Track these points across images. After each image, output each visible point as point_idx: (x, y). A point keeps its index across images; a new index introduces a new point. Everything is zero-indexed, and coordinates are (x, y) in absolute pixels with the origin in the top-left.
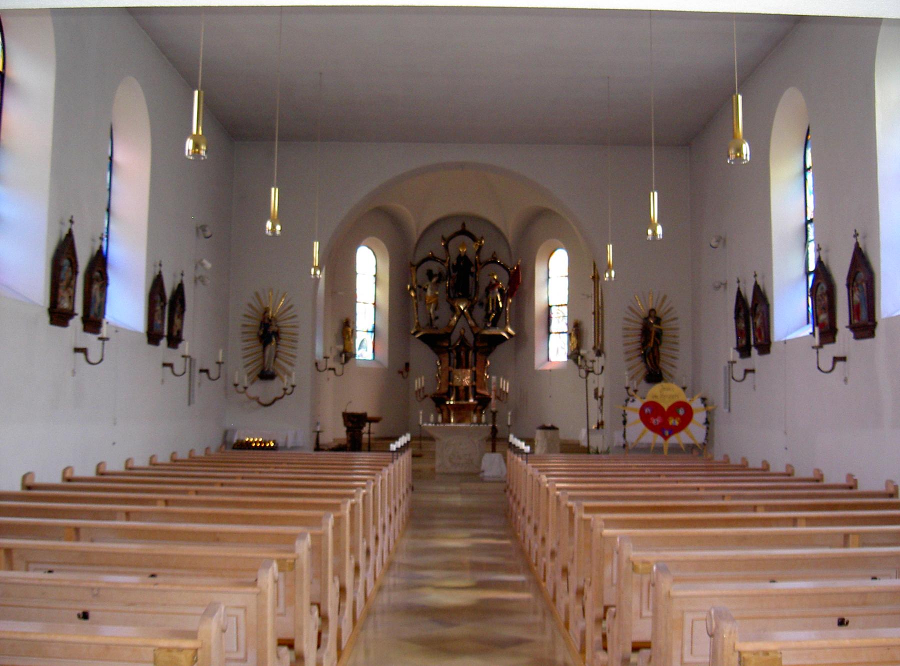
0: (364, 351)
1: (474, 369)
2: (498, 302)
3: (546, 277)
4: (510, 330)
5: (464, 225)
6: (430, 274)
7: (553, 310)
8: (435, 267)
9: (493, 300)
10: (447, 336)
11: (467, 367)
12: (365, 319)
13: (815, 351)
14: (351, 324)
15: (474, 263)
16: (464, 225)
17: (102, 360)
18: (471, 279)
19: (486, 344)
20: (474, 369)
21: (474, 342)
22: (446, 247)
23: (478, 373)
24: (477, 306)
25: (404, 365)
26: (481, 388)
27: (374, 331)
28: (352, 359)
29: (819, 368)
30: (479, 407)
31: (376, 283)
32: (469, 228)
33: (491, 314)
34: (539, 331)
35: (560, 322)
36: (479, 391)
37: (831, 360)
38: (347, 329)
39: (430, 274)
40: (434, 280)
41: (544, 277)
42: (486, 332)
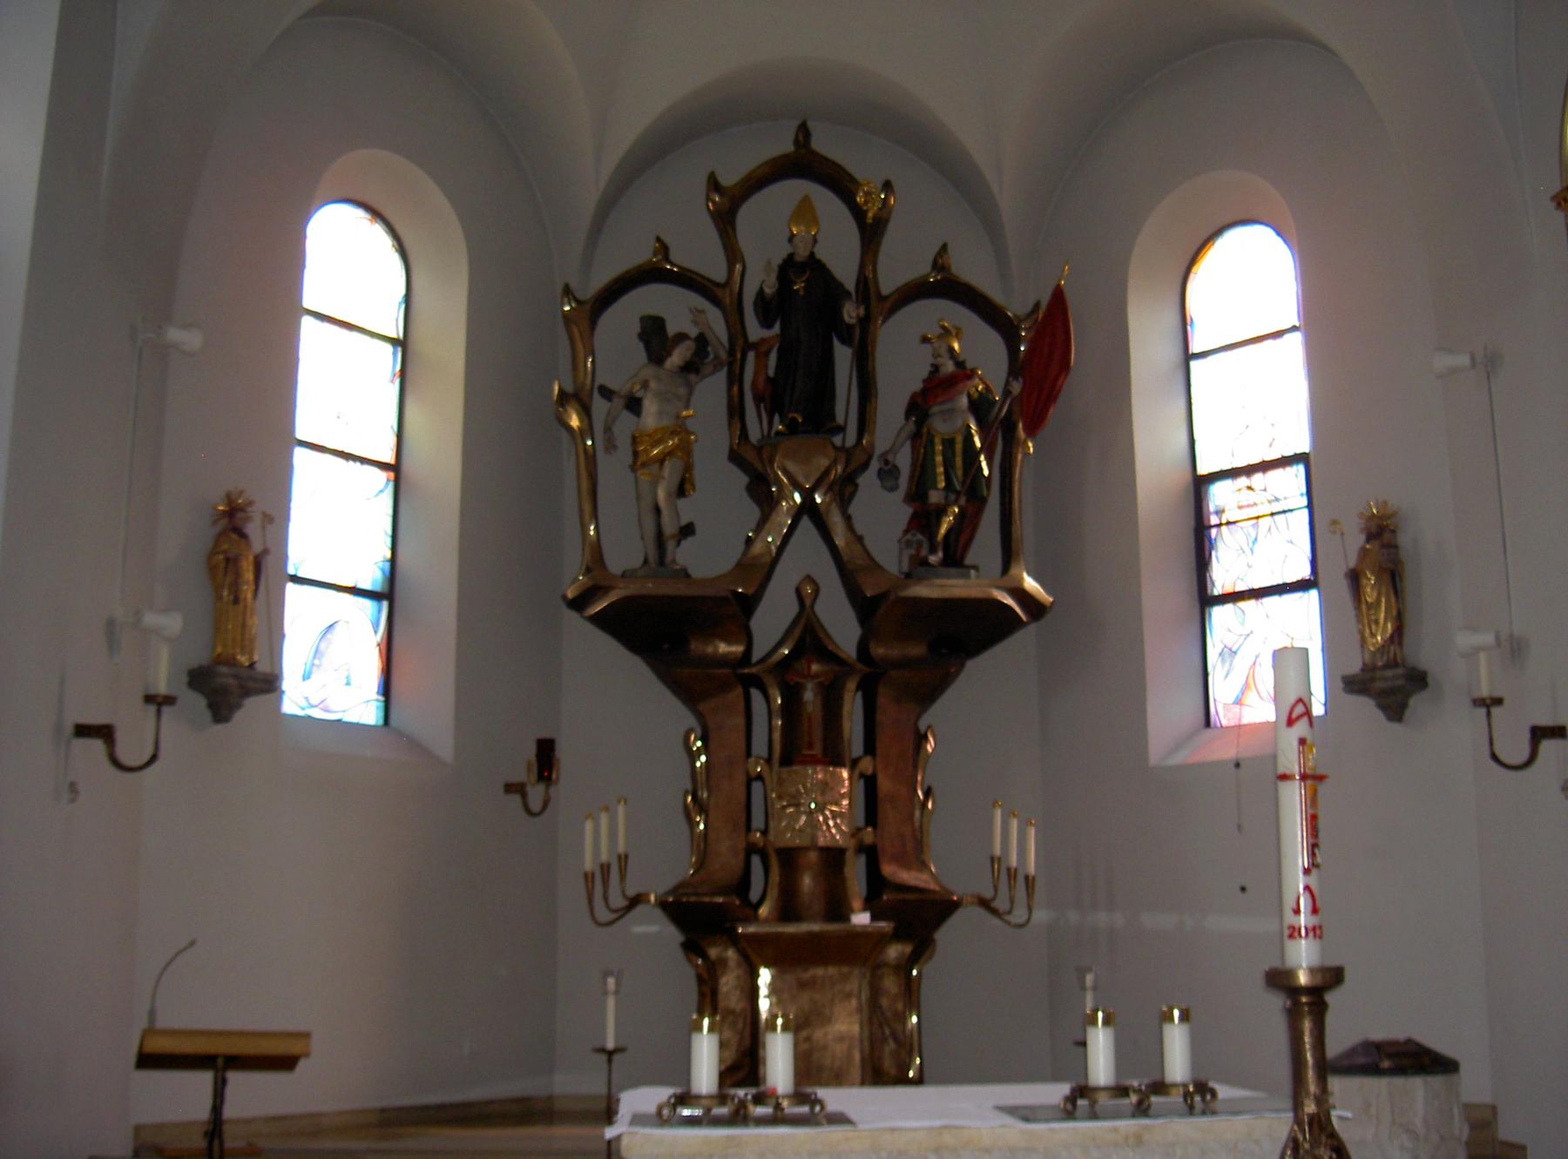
0: (329, 664)
1: (867, 765)
2: (971, 455)
3: (1173, 353)
4: (1030, 583)
5: (804, 132)
6: (654, 336)
7: (1220, 495)
8: (678, 309)
9: (949, 444)
10: (734, 609)
11: (834, 756)
12: (336, 525)
13: (1483, 711)
14: (253, 529)
15: (850, 285)
16: (804, 132)
17: (154, 758)
18: (843, 356)
19: (917, 650)
20: (867, 765)
21: (863, 647)
22: (725, 220)
23: (884, 784)
24: (868, 481)
25: (531, 752)
26: (903, 861)
27: (387, 594)
28: (252, 704)
29: (1494, 757)
30: (894, 952)
31: (403, 374)
32: (825, 144)
33: (941, 511)
34: (1160, 592)
35: (1263, 538)
36: (889, 870)
37: (1527, 736)
38: (238, 556)
39: (654, 336)
40: (677, 358)
41: (1168, 353)
42: (921, 591)
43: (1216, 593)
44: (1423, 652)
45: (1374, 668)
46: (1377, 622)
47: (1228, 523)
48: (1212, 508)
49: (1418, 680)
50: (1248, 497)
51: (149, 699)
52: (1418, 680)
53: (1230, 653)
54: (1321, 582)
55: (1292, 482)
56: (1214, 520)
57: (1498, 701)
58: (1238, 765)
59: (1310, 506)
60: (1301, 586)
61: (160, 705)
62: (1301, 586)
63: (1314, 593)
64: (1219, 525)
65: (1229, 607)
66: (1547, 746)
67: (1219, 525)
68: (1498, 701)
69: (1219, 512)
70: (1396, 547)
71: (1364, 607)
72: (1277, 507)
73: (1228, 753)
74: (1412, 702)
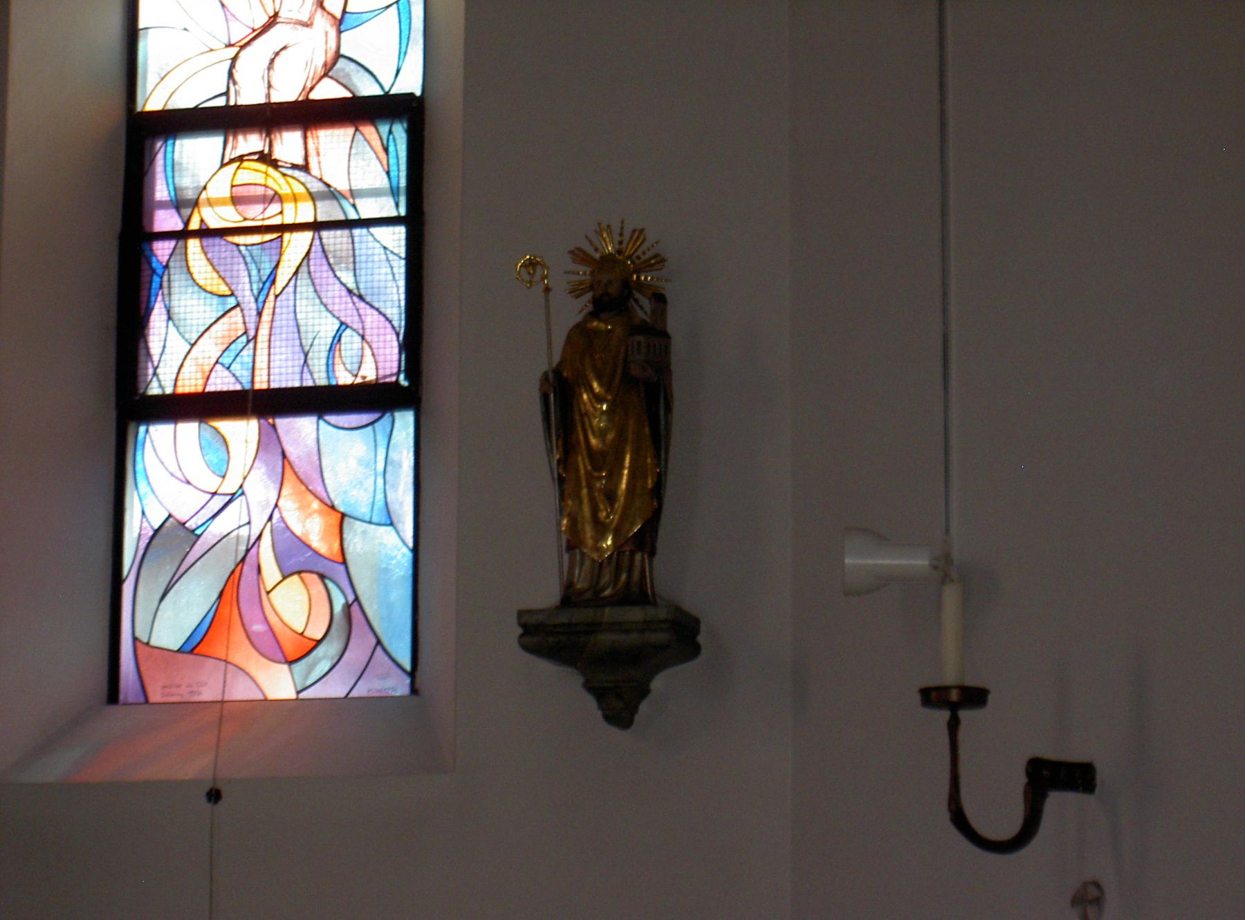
7: (193, 165)
29: (959, 820)
43: (154, 390)
44: (688, 572)
45: (596, 600)
46: (611, 497)
47: (205, 233)
48: (161, 192)
49: (683, 636)
50: (254, 174)
51: (932, 696)
52: (683, 636)
53: (176, 538)
54: (429, 396)
55: (360, 165)
56: (166, 221)
57: (975, 697)
58: (214, 795)
59: (415, 221)
60: (369, 399)
61: (954, 708)
62: (369, 399)
63: (405, 422)
64: (183, 235)
65: (189, 430)
66: (1057, 803)
67: (183, 235)
68: (975, 697)
69: (181, 204)
70: (665, 335)
71: (582, 464)
72: (329, 211)
73: (195, 767)
74: (658, 683)
